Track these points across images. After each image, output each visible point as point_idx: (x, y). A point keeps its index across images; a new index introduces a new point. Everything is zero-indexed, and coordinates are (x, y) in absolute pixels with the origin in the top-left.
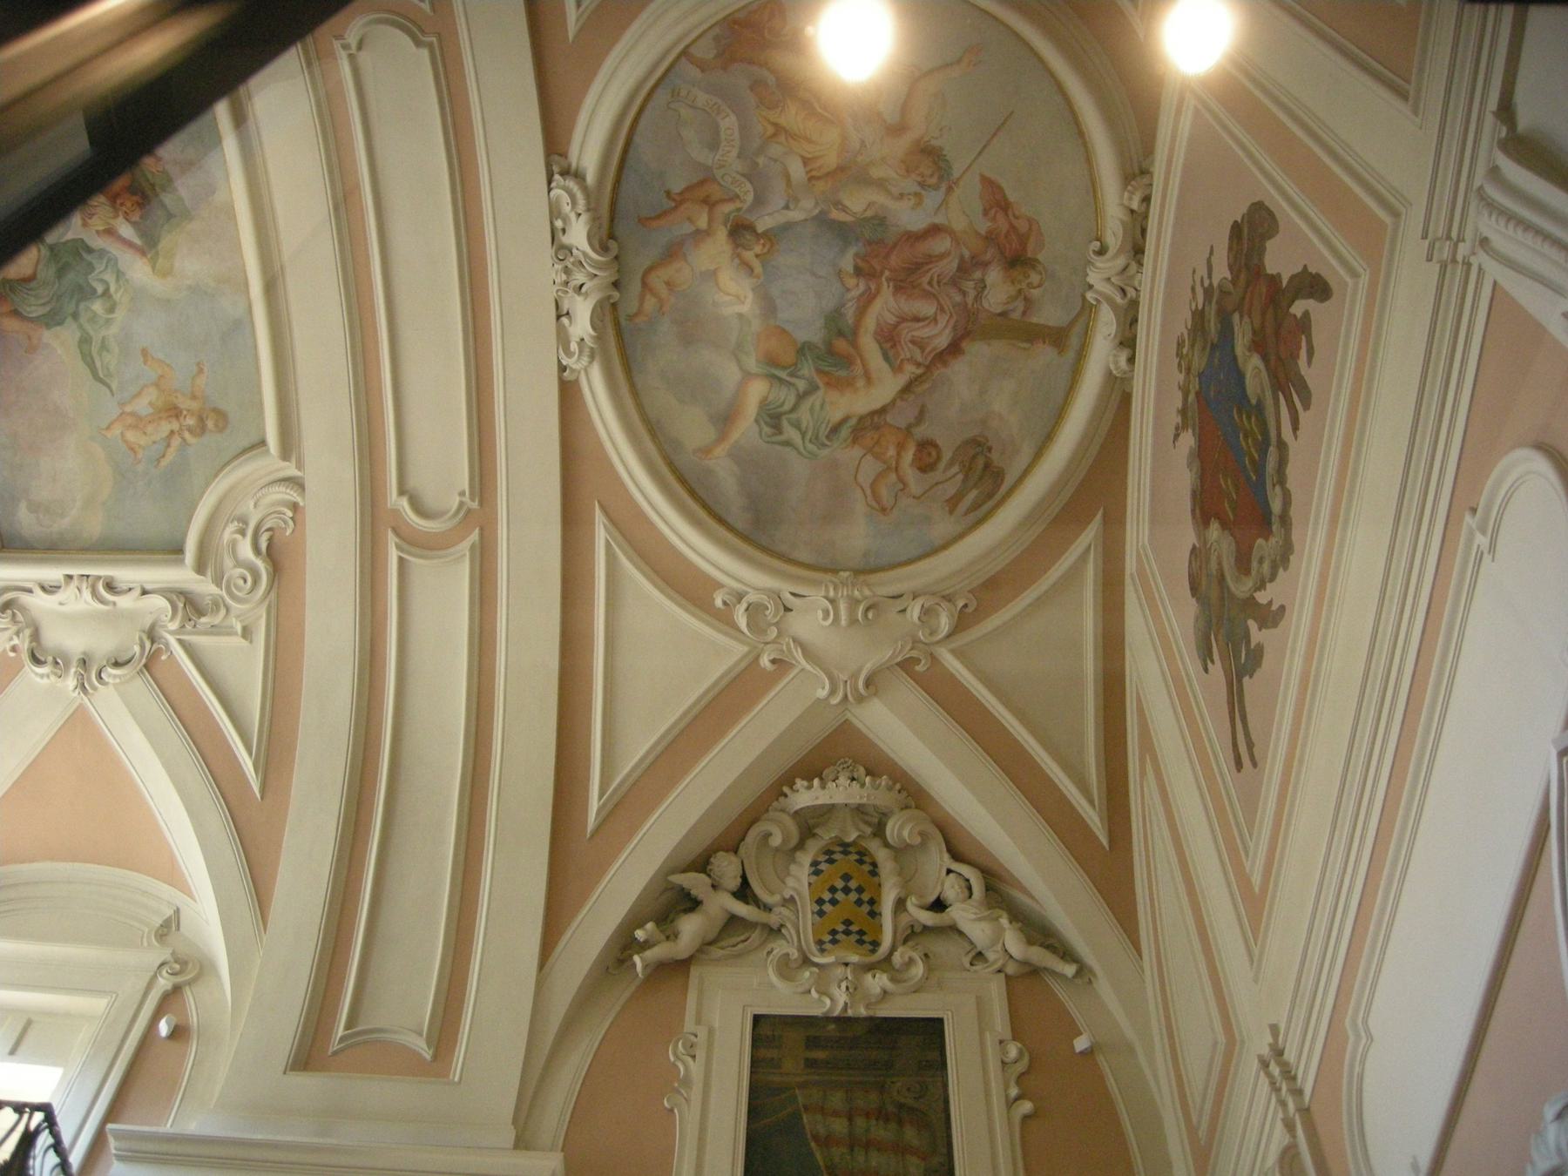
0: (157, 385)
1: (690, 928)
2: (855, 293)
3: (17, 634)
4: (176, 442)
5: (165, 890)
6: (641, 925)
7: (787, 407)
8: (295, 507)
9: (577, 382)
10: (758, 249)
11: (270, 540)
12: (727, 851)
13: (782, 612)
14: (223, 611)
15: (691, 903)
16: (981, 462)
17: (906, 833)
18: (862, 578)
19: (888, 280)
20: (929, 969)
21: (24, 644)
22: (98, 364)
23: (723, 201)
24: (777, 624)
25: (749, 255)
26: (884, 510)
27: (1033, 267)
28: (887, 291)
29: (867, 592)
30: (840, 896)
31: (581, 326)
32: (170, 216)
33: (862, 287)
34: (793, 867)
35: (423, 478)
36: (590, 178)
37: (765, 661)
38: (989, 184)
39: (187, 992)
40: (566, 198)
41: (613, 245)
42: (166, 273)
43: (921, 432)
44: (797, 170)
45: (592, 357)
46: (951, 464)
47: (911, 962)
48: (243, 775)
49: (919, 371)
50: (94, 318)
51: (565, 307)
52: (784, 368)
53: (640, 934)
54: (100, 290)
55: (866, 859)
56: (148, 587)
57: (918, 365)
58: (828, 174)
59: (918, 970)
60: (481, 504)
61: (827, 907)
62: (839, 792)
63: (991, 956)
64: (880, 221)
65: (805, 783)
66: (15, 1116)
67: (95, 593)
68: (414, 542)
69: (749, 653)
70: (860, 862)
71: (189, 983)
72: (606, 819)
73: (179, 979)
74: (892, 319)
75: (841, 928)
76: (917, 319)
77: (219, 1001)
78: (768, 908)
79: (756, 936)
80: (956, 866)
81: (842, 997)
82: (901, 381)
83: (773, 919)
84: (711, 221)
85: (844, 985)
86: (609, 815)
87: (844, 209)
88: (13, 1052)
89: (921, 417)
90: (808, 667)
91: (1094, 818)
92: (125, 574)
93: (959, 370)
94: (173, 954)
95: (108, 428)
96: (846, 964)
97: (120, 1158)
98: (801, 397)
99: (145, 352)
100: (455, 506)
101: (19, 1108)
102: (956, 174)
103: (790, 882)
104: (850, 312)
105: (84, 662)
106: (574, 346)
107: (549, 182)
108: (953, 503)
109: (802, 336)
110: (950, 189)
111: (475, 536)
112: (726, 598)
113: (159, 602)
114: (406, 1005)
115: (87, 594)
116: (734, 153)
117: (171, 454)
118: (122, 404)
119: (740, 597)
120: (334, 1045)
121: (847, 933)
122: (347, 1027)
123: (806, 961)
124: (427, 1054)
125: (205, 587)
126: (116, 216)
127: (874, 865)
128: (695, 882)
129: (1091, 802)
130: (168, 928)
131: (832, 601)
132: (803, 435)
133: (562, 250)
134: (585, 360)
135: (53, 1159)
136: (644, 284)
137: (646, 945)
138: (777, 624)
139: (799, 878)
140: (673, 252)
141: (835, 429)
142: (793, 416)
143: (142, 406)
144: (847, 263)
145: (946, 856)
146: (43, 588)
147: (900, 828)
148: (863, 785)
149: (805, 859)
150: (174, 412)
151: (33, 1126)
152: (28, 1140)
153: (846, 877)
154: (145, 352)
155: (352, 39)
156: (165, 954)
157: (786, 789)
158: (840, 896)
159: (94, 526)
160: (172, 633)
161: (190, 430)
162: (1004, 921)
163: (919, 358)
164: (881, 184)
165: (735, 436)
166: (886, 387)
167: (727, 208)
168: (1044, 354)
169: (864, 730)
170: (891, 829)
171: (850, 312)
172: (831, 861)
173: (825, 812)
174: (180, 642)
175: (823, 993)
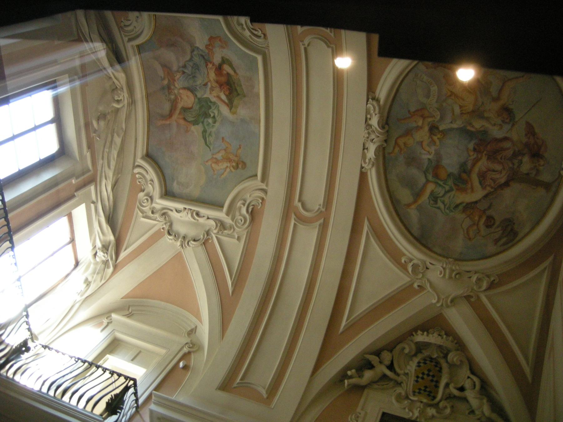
0: (225, 150)
1: (368, 375)
2: (472, 158)
3: (165, 224)
4: (228, 170)
5: (194, 319)
6: (350, 370)
7: (441, 195)
8: (263, 199)
9: (366, 173)
10: (439, 136)
11: (253, 209)
12: (388, 351)
13: (425, 269)
14: (232, 230)
15: (370, 366)
16: (509, 229)
17: (455, 359)
18: (457, 262)
19: (485, 155)
20: (453, 411)
21: (167, 228)
22: (207, 139)
23: (428, 117)
24: (422, 273)
25: (435, 138)
26: (470, 239)
27: (541, 158)
28: (484, 159)
29: (457, 268)
30: (425, 377)
31: (371, 154)
32: (238, 95)
33: (475, 156)
34: (411, 362)
35: (307, 198)
36: (382, 102)
37: (415, 285)
38: (528, 124)
39: (192, 356)
40: (372, 108)
41: (387, 127)
42: (234, 113)
43: (489, 213)
44: (457, 110)
45: (373, 165)
46: (498, 227)
47: (446, 407)
48: (228, 286)
49: (492, 190)
50: (209, 124)
51: (367, 146)
52: (441, 180)
53: (349, 373)
54: (212, 115)
55: (438, 365)
56: (210, 217)
57: (492, 188)
58: (468, 113)
59: (448, 411)
60: (326, 210)
61: (420, 380)
62: (433, 338)
63: (477, 412)
64: (485, 132)
65: (421, 333)
66: (125, 380)
67: (192, 216)
68: (301, 219)
69: (410, 281)
70: (436, 366)
71: (194, 352)
72: (347, 329)
73: (190, 350)
74: (484, 169)
75: (423, 388)
76: (494, 171)
77: (200, 361)
78: (398, 375)
79: (392, 384)
80: (472, 376)
81: (416, 414)
82: (485, 193)
83: (399, 379)
84: (423, 123)
85: (418, 409)
86: (348, 328)
87: (473, 127)
88: (132, 360)
89: (489, 208)
90: (430, 290)
91: (527, 370)
92: (204, 211)
93: (507, 193)
94: (191, 340)
95: (207, 162)
96: (421, 402)
97: (155, 403)
98: (446, 192)
99: (223, 139)
100: (317, 209)
101: (127, 378)
102: (517, 120)
103: (408, 367)
104: (469, 164)
105: (184, 238)
106: (367, 161)
107: (367, 101)
108: (496, 241)
109: (450, 170)
110: (513, 125)
111: (322, 221)
112: (406, 260)
113: (212, 223)
114: (262, 377)
115: (190, 215)
116: (435, 100)
117: (226, 174)
118: (213, 154)
119: (411, 260)
120: (235, 385)
121: (425, 391)
122: (241, 380)
123: (407, 397)
124: (265, 396)
125: (228, 220)
126: (221, 92)
127: (441, 368)
128: (374, 359)
129: (528, 363)
130: (192, 332)
131: (444, 269)
132: (445, 206)
133: (368, 126)
134: (370, 166)
135: (133, 397)
136: (396, 143)
137: (351, 377)
138: (422, 273)
139: (412, 367)
140: (408, 133)
141: (457, 206)
142: (442, 199)
143: (219, 156)
144: (471, 146)
145: (469, 372)
146: (176, 211)
147: (453, 357)
148: (442, 338)
149: (416, 360)
150: (230, 160)
151: (129, 385)
152: (127, 389)
153: (429, 370)
154: (223, 139)
155: (306, 42)
156: (188, 340)
157: (414, 333)
158: (425, 377)
159: (196, 193)
160: (214, 234)
161: (233, 167)
162: (485, 401)
163: (493, 185)
164: (488, 119)
165: (420, 202)
166: (478, 194)
167: (430, 120)
168: (541, 191)
169: (447, 317)
170: (450, 356)
171: (469, 164)
172: (425, 363)
173: (427, 345)
174: (217, 237)
175: (410, 410)
